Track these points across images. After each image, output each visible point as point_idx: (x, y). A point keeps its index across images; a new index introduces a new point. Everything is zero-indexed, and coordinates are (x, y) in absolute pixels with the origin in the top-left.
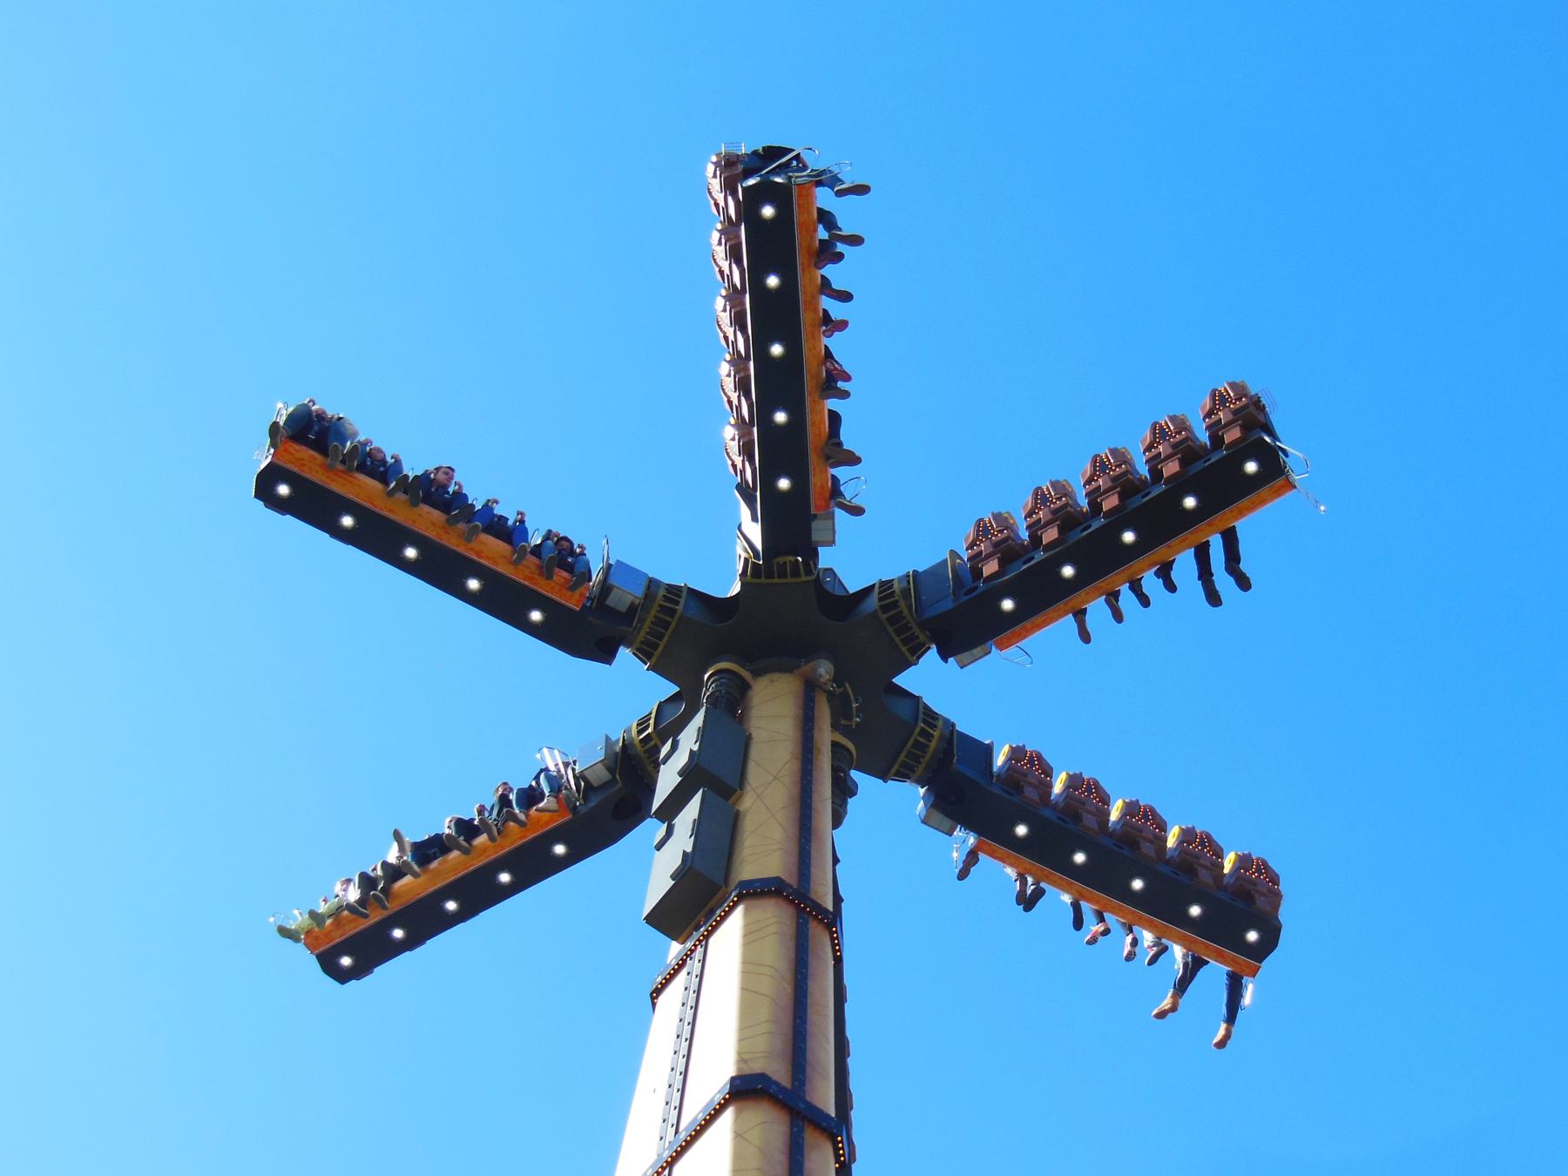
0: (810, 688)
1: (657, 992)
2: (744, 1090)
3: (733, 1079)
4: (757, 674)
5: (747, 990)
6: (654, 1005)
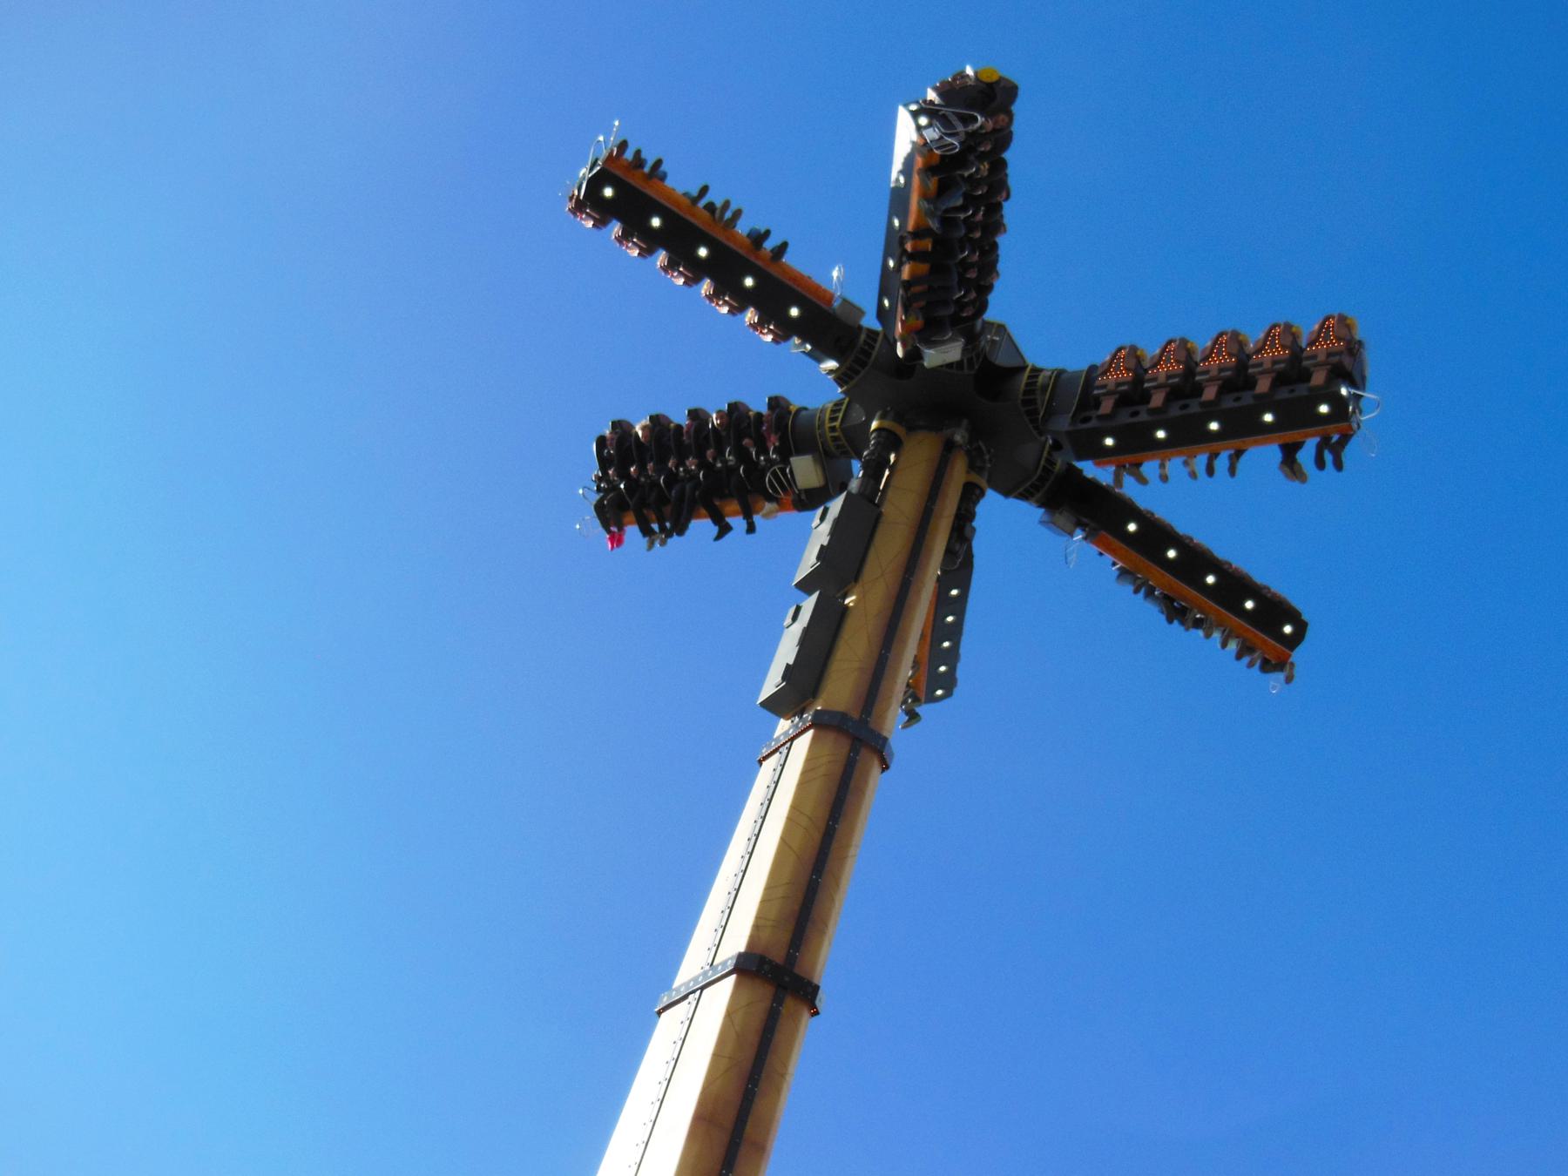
0: (949, 446)
1: (765, 758)
2: (749, 967)
3: (740, 956)
4: (911, 429)
5: (769, 888)
6: (761, 764)
